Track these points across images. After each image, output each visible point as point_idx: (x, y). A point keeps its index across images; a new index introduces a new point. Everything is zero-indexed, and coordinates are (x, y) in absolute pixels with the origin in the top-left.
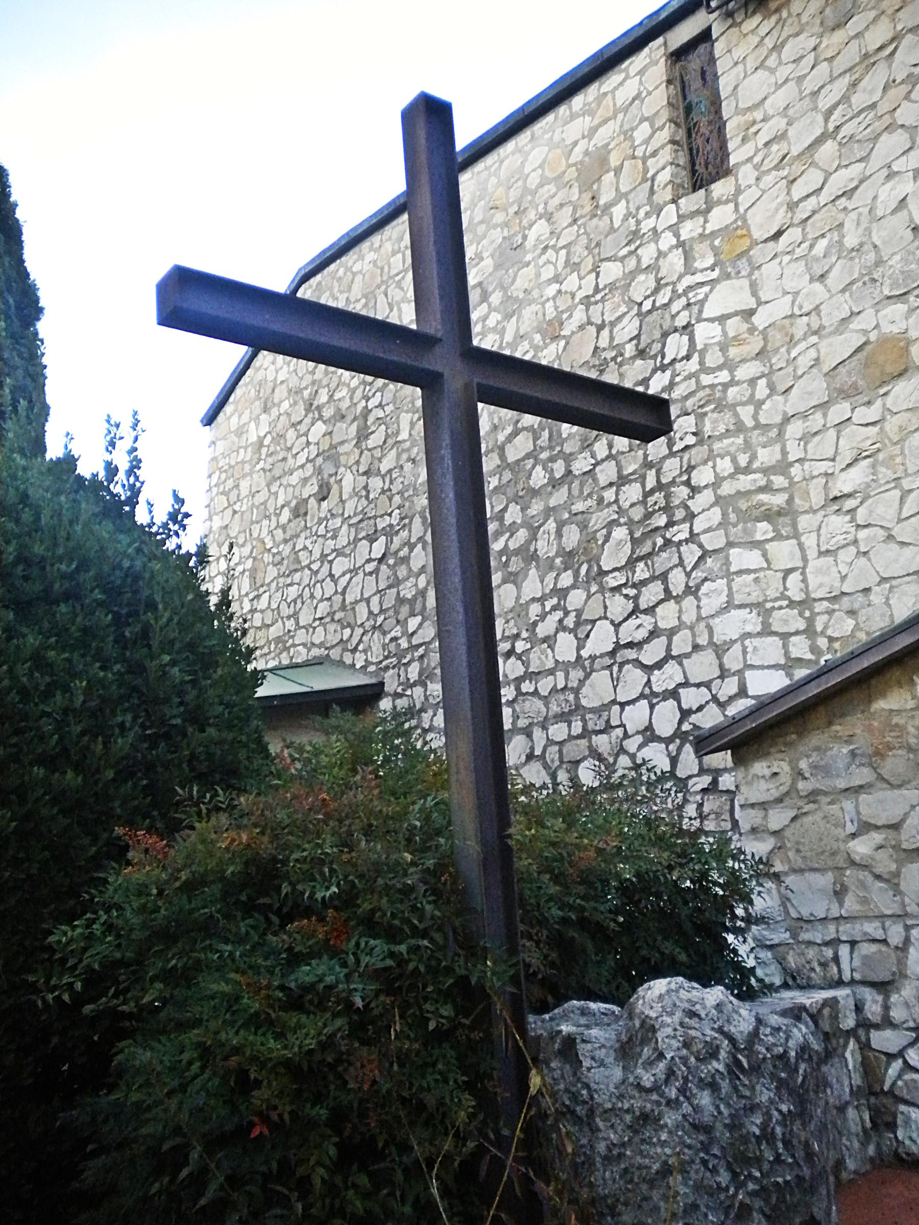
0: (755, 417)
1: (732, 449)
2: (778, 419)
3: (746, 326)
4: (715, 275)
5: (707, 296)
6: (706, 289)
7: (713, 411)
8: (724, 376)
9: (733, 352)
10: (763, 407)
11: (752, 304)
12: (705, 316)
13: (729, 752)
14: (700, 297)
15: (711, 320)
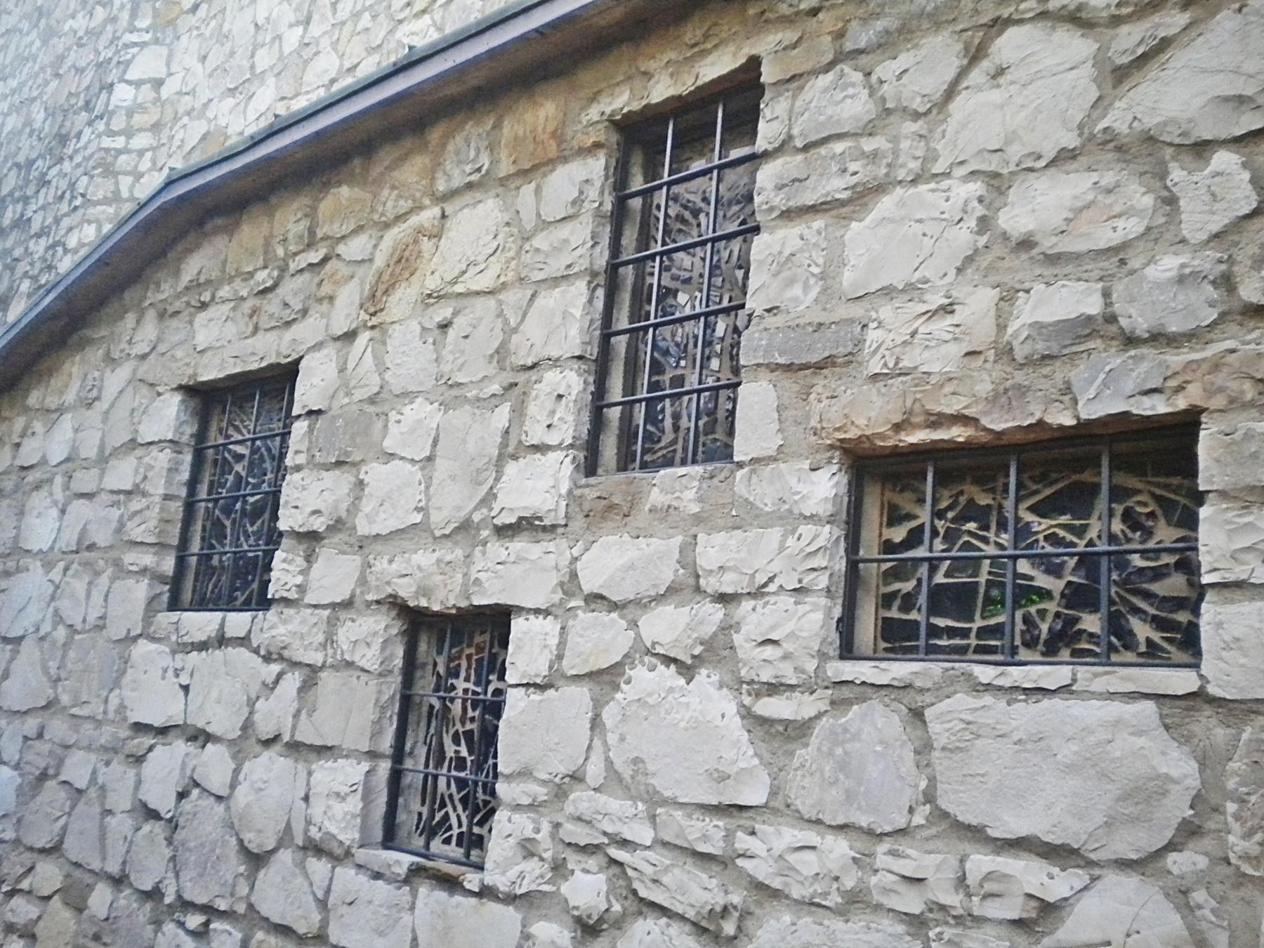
0: (131, 189)
1: (102, 217)
2: (706, 678)
3: (154, 95)
4: (147, 37)
5: (134, 57)
6: (136, 50)
7: (98, 175)
8: (120, 142)
9: (137, 117)
10: (142, 180)
11: (162, 73)
12: (127, 77)
13: (269, 596)
14: (129, 57)
15: (129, 83)
